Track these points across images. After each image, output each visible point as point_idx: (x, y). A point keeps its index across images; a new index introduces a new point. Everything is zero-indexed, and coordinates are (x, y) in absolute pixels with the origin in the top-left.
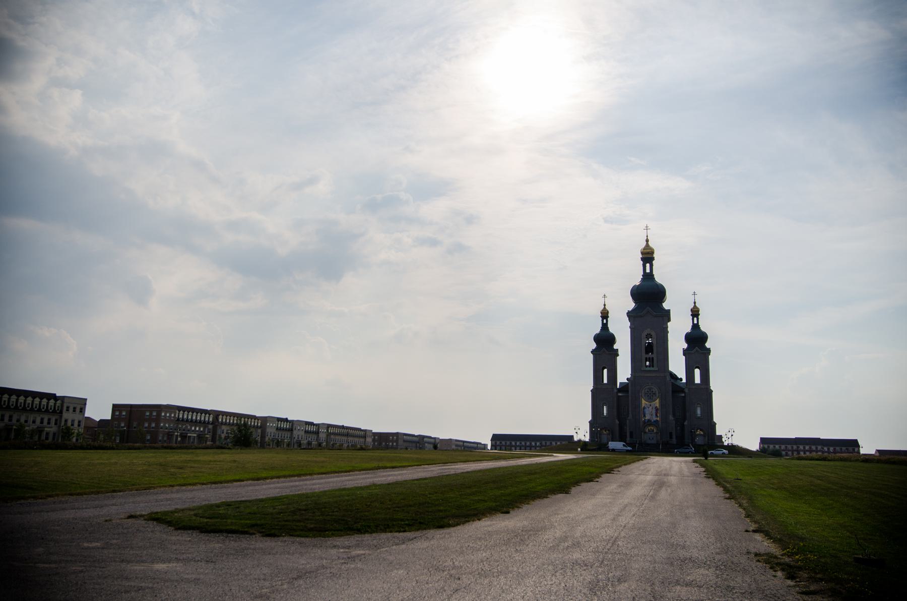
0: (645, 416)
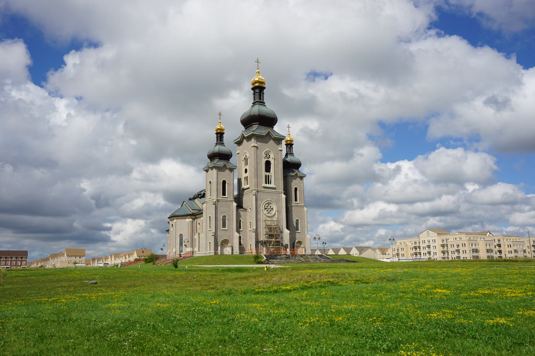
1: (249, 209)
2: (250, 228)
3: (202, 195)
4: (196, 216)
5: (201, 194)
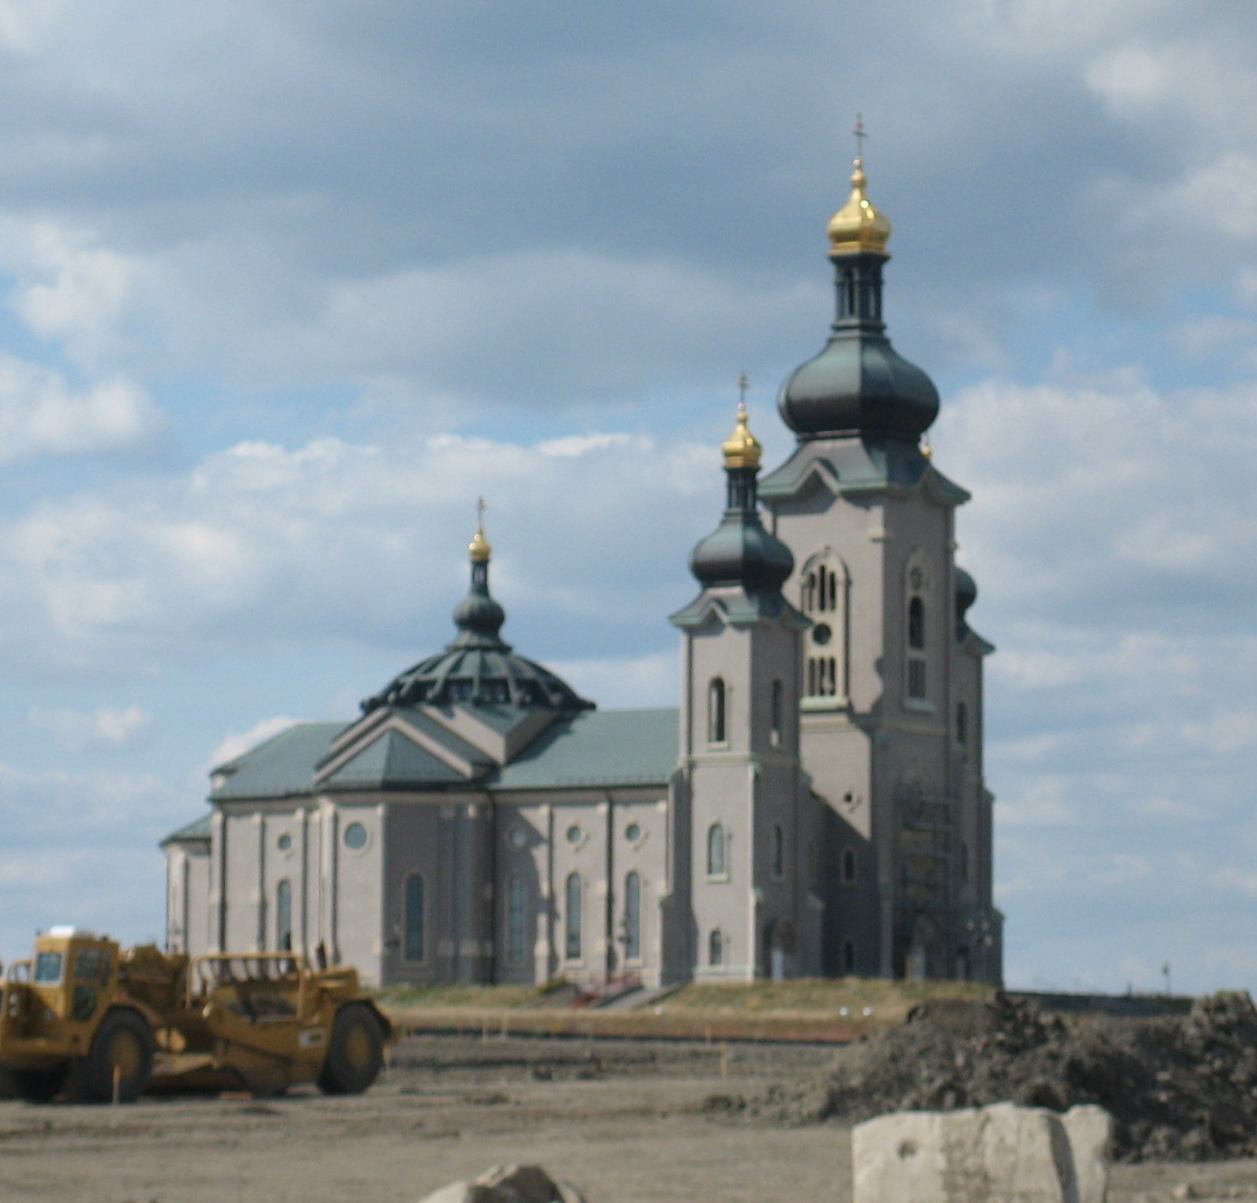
2: (849, 874)
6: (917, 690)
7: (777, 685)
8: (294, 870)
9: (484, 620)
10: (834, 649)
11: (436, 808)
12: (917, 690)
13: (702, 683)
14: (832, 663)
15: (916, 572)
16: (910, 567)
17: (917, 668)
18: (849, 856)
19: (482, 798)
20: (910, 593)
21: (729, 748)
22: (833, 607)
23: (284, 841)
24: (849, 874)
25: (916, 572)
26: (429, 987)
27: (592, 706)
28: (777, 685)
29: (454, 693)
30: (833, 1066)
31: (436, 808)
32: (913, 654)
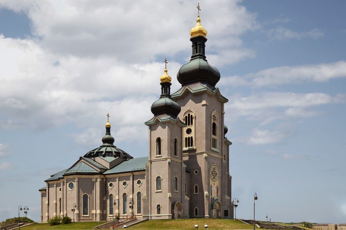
0: (211, 194)
1: (194, 172)
2: (196, 192)
3: (94, 154)
4: (106, 176)
5: (93, 153)
6: (214, 146)
7: (176, 140)
8: (61, 197)
9: (109, 141)
10: (192, 135)
11: (91, 179)
12: (214, 146)
13: (154, 140)
14: (192, 137)
15: (214, 116)
16: (212, 115)
17: (214, 141)
18: (196, 187)
19: (102, 176)
20: (213, 121)
21: (161, 157)
22: (192, 124)
23: (60, 190)
24: (196, 192)
25: (214, 116)
26: (65, 224)
27: (132, 158)
28: (176, 140)
29: (99, 154)
30: (168, 162)
31: (91, 179)
32: (213, 136)
